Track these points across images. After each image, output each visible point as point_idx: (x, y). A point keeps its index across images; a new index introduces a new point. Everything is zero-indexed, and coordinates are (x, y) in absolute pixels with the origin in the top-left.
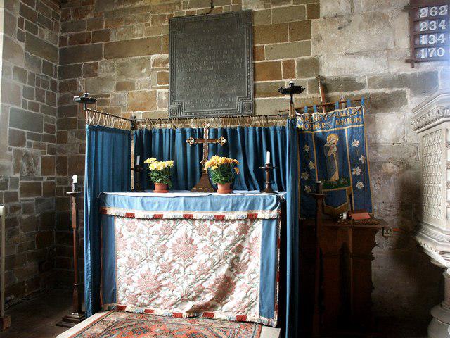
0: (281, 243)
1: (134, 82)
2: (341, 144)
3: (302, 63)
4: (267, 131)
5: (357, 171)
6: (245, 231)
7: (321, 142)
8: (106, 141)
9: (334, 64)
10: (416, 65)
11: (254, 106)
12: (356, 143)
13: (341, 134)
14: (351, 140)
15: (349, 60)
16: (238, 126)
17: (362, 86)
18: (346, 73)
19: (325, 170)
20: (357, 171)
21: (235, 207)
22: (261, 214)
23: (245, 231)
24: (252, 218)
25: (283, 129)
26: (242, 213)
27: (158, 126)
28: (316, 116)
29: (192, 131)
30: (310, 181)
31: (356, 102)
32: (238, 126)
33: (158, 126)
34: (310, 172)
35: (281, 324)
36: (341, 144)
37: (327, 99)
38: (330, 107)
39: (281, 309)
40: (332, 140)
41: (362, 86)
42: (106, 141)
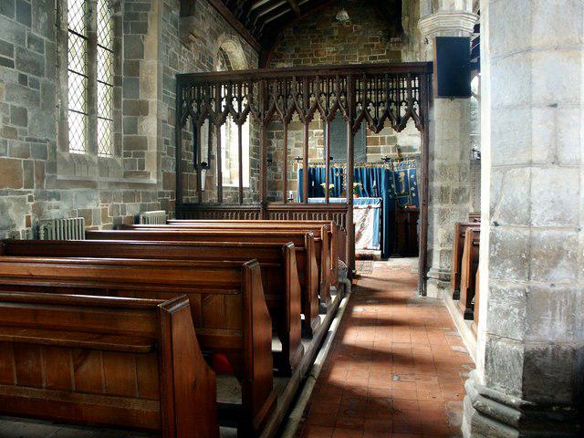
0: (381, 217)
1: (177, 76)
2: (406, 177)
3: (389, 138)
4: (372, 170)
5: (413, 189)
6: (367, 212)
7: (397, 175)
8: (76, 124)
9: (403, 140)
10: (312, 373)
11: (366, 158)
12: (412, 176)
13: (406, 172)
14: (410, 175)
15: (410, 137)
16: (359, 167)
17: (415, 150)
18: (409, 144)
19: (399, 189)
20: (413, 189)
21: (363, 203)
22: (373, 205)
23: (367, 212)
24: (370, 207)
25: (380, 169)
26: (366, 206)
27: (318, 166)
28: (395, 163)
29: (337, 170)
30: (392, 193)
31: (412, 158)
32: (359, 167)
33: (318, 166)
34: (392, 189)
35: (381, 249)
36: (406, 177)
37: (400, 156)
38: (402, 160)
39: (381, 243)
40: (402, 175)
41: (415, 150)
42: (76, 124)
